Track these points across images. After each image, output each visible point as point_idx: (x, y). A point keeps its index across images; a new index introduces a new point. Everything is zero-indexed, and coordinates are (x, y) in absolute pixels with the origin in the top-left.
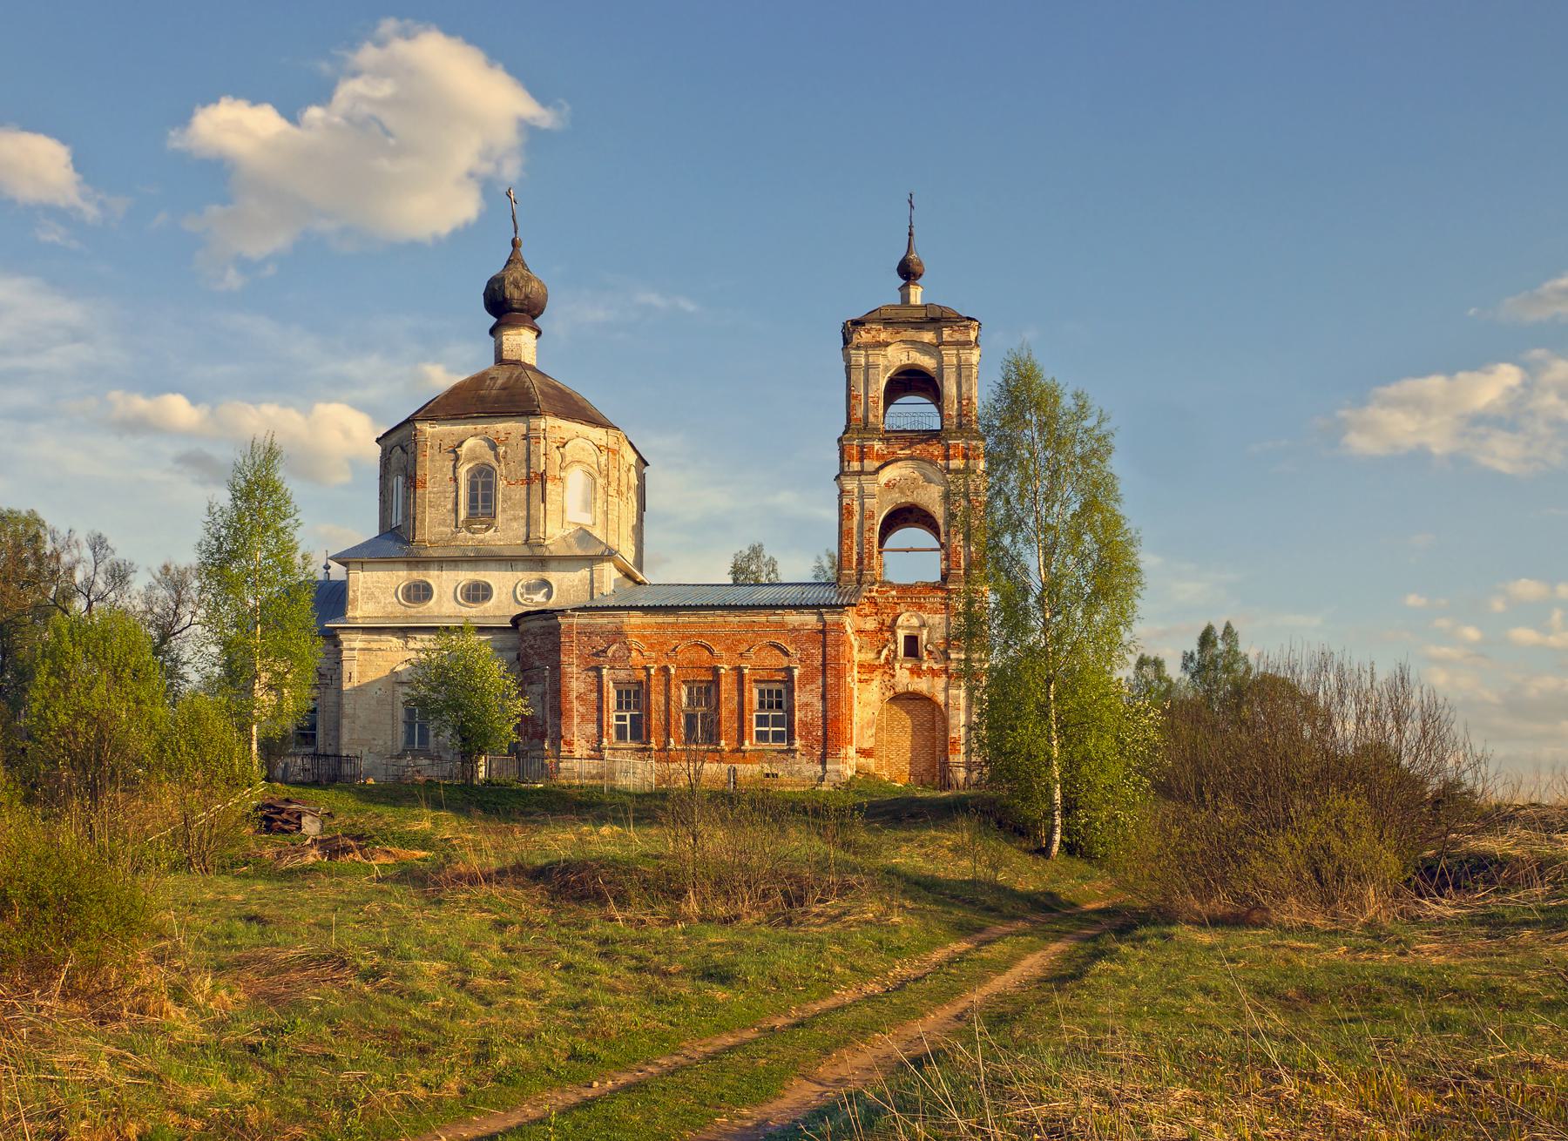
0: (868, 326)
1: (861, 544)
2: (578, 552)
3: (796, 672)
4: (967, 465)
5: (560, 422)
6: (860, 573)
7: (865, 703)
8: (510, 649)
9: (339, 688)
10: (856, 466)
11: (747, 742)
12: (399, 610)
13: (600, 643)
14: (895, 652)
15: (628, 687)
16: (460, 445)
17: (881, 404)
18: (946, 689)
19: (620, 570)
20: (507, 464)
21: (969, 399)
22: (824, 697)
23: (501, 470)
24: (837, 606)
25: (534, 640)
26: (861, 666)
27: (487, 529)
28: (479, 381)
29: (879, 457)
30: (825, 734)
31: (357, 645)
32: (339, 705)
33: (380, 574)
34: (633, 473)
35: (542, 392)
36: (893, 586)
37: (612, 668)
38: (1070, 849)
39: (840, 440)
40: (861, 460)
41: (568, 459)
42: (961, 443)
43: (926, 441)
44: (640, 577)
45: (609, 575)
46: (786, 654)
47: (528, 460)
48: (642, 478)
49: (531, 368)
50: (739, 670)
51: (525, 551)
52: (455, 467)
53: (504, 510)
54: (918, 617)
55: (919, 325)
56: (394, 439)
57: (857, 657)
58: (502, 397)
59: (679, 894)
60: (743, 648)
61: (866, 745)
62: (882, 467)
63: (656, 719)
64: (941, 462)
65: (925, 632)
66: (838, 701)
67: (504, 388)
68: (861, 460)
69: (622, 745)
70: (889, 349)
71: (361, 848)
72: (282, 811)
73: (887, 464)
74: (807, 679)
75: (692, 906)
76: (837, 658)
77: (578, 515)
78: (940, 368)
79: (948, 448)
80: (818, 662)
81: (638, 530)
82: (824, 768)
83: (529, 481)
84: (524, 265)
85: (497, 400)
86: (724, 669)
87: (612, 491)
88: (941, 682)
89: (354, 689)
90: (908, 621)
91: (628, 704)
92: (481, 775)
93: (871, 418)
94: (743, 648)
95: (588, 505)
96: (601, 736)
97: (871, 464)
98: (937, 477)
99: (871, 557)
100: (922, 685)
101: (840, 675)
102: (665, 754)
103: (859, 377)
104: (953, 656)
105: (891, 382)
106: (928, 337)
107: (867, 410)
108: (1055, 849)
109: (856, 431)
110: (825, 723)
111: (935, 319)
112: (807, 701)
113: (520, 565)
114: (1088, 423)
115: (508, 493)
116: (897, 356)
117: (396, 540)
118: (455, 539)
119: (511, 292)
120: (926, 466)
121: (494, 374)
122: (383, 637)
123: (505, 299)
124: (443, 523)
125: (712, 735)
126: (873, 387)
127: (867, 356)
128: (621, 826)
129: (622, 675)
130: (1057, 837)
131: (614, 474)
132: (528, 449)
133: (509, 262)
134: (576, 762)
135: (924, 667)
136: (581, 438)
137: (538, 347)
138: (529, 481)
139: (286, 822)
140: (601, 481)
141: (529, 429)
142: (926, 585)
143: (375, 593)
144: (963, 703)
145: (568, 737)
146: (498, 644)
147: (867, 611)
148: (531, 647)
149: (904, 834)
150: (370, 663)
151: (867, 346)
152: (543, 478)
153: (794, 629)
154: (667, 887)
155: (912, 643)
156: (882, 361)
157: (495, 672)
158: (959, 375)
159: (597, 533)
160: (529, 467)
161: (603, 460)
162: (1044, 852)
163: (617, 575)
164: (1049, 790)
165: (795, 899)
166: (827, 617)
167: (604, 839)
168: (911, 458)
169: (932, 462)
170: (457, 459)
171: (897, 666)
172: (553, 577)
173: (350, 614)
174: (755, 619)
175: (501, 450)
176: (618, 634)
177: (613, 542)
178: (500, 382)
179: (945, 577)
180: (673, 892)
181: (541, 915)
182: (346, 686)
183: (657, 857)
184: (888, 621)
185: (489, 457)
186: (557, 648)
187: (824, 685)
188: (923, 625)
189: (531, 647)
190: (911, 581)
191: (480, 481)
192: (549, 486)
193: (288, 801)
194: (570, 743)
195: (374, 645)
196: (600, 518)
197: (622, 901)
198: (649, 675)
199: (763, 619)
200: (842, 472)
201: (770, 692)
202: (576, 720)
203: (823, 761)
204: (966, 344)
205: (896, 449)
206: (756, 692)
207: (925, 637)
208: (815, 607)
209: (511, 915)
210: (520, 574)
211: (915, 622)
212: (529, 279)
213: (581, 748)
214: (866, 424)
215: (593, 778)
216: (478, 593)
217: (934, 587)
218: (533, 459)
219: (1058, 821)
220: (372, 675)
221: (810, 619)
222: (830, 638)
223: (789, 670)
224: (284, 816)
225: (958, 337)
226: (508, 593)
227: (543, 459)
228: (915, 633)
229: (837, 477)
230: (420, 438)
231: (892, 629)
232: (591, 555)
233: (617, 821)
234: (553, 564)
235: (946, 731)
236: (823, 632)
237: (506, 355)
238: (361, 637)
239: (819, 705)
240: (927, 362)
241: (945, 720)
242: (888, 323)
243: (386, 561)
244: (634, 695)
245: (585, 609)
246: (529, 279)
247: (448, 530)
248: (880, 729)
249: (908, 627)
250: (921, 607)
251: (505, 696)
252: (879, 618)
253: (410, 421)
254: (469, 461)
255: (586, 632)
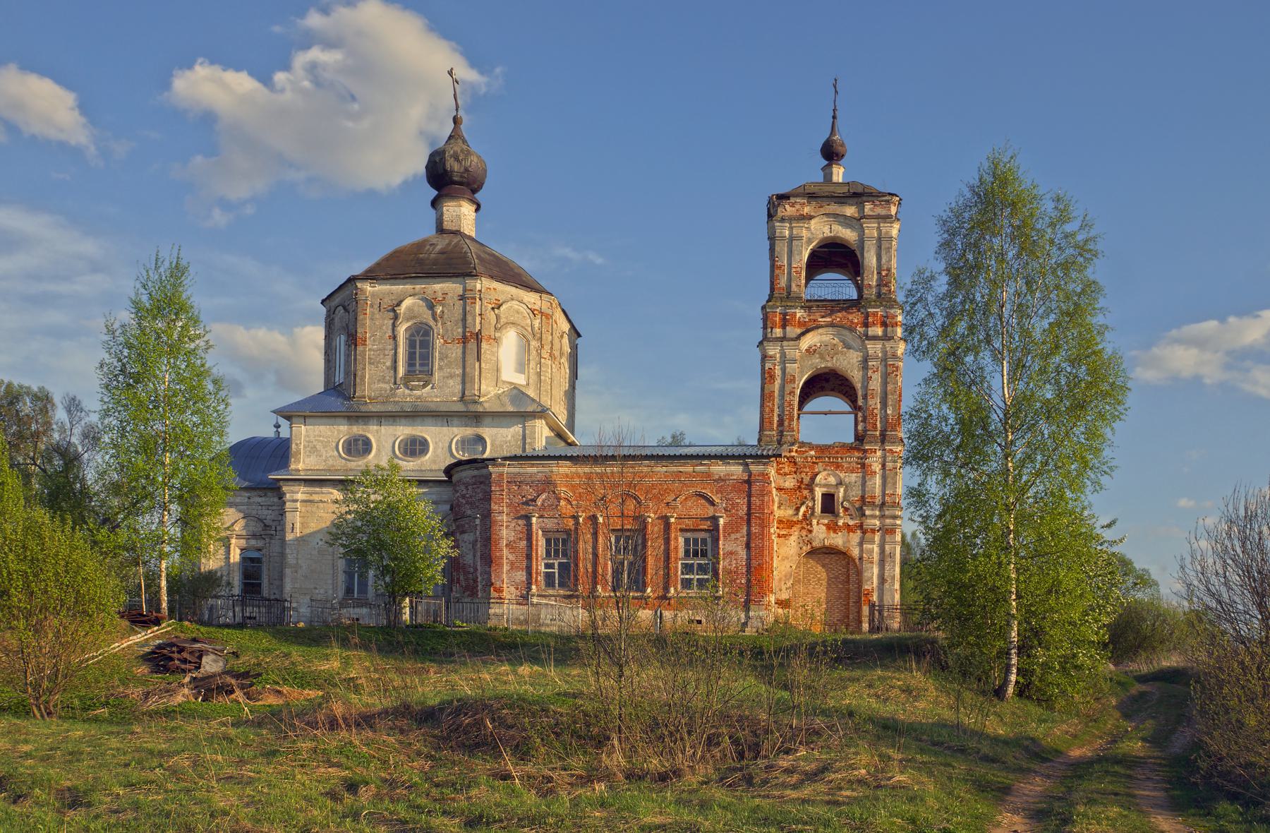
0: (792, 200)
1: (781, 407)
2: (511, 409)
3: (721, 521)
4: (885, 332)
5: (495, 284)
6: (781, 434)
7: (785, 555)
8: (446, 502)
9: (283, 540)
10: (778, 332)
11: (672, 590)
12: (340, 464)
13: (530, 492)
14: (813, 508)
15: (557, 535)
16: (399, 305)
17: (804, 274)
18: (861, 544)
19: (551, 429)
20: (443, 324)
21: (889, 270)
22: (748, 546)
23: (438, 328)
24: (762, 456)
25: (466, 486)
26: (780, 522)
27: (424, 386)
28: (420, 246)
29: (801, 324)
30: (749, 581)
31: (300, 496)
32: (282, 555)
33: (322, 428)
34: (566, 340)
35: (479, 257)
36: (811, 447)
37: (541, 517)
38: (1021, 692)
39: (763, 308)
40: (784, 327)
41: (503, 320)
42: (880, 311)
43: (846, 309)
44: (572, 438)
45: (541, 435)
46: (712, 503)
47: (464, 319)
48: (574, 348)
49: (470, 238)
50: (665, 519)
51: (460, 407)
52: (394, 326)
53: (441, 368)
54: (835, 476)
55: (842, 199)
56: (337, 300)
57: (778, 513)
58: (448, 261)
59: (601, 741)
60: (670, 498)
61: (784, 596)
62: (803, 334)
63: (585, 566)
64: (860, 329)
65: (842, 490)
66: (762, 549)
67: (442, 252)
68: (784, 327)
69: (551, 592)
70: (813, 222)
71: (242, 687)
72: (181, 650)
73: (808, 331)
74: (732, 528)
75: (615, 759)
76: (761, 507)
77: (511, 375)
78: (861, 241)
79: (867, 316)
80: (743, 511)
81: (571, 395)
82: (748, 617)
83: (464, 340)
84: (464, 141)
85: (435, 262)
86: (651, 517)
87: (545, 354)
88: (855, 537)
89: (297, 539)
90: (825, 479)
91: (557, 552)
92: (406, 616)
93: (794, 288)
94: (670, 498)
95: (521, 368)
96: (529, 584)
97: (792, 331)
98: (856, 343)
99: (791, 419)
100: (838, 540)
101: (764, 525)
102: (591, 601)
103: (782, 248)
104: (867, 513)
105: (813, 255)
106: (850, 211)
107: (790, 279)
108: (1011, 690)
109: (779, 296)
110: (749, 571)
111: (857, 195)
112: (731, 548)
113: (456, 421)
114: (1068, 228)
115: (444, 350)
116: (819, 229)
117: (339, 397)
118: (394, 395)
119: (451, 164)
120: (846, 333)
121: (434, 241)
122: (324, 490)
123: (445, 170)
124: (382, 380)
125: (639, 582)
126: (796, 257)
127: (791, 228)
128: (542, 666)
129: (550, 524)
130: (1013, 678)
131: (547, 337)
132: (464, 309)
133: (450, 137)
134: (505, 610)
135: (841, 523)
136: (519, 302)
137: (476, 219)
138: (464, 340)
139: (185, 661)
140: (534, 344)
141: (465, 290)
142: (843, 446)
143: (316, 446)
144: (876, 557)
145: (498, 584)
146: (434, 497)
147: (787, 470)
148: (463, 497)
149: (846, 674)
150: (310, 514)
151: (791, 219)
152: (478, 337)
153: (720, 479)
154: (586, 732)
155: (829, 499)
156: (804, 233)
157: (424, 513)
158: (879, 247)
159: (531, 393)
160: (465, 327)
161: (537, 323)
162: (999, 693)
163: (547, 432)
164: (1003, 633)
165: (749, 749)
166: (752, 468)
167: (518, 679)
168: (831, 325)
169: (852, 329)
170: (396, 317)
171: (815, 522)
172: (488, 433)
173: (293, 467)
174: (681, 469)
175: (439, 309)
176: (547, 484)
177: (546, 401)
178: (439, 247)
179: (860, 438)
180: (592, 738)
181: (413, 770)
182: (289, 537)
183: (575, 696)
184: (807, 480)
185: (427, 316)
186: (487, 497)
187: (749, 534)
188: (840, 483)
189: (463, 497)
190: (830, 442)
191: (418, 339)
192: (484, 345)
193: (195, 640)
194: (500, 590)
195: (316, 497)
196: (533, 378)
197: (523, 752)
198: (577, 523)
199: (690, 469)
200: (765, 338)
201: (696, 541)
202: (506, 568)
203: (746, 607)
204: (887, 218)
205: (817, 316)
206: (681, 540)
207: (841, 495)
208: (741, 458)
209: (373, 772)
210: (455, 430)
211: (832, 480)
212: (469, 153)
213: (509, 592)
214: (789, 293)
215: (521, 623)
216: (415, 447)
217: (851, 448)
218: (469, 319)
219: (1014, 661)
220: (314, 526)
221: (736, 470)
222: (755, 488)
223: (715, 519)
224: (185, 655)
225: (880, 211)
226: (443, 445)
227: (478, 319)
228: (832, 491)
229: (761, 343)
230: (361, 297)
231: (810, 487)
232: (522, 411)
233: (535, 660)
234: (487, 420)
235: (860, 584)
236: (749, 482)
237: (447, 225)
238: (302, 489)
239: (743, 553)
240: (849, 235)
241: (859, 573)
242: (812, 196)
243: (328, 415)
244: (562, 543)
245: (514, 458)
246: (469, 153)
247: (387, 386)
248: (797, 581)
249: (825, 486)
250: (838, 466)
251: (431, 538)
252: (798, 476)
253: (352, 280)
254: (408, 320)
255: (515, 481)
